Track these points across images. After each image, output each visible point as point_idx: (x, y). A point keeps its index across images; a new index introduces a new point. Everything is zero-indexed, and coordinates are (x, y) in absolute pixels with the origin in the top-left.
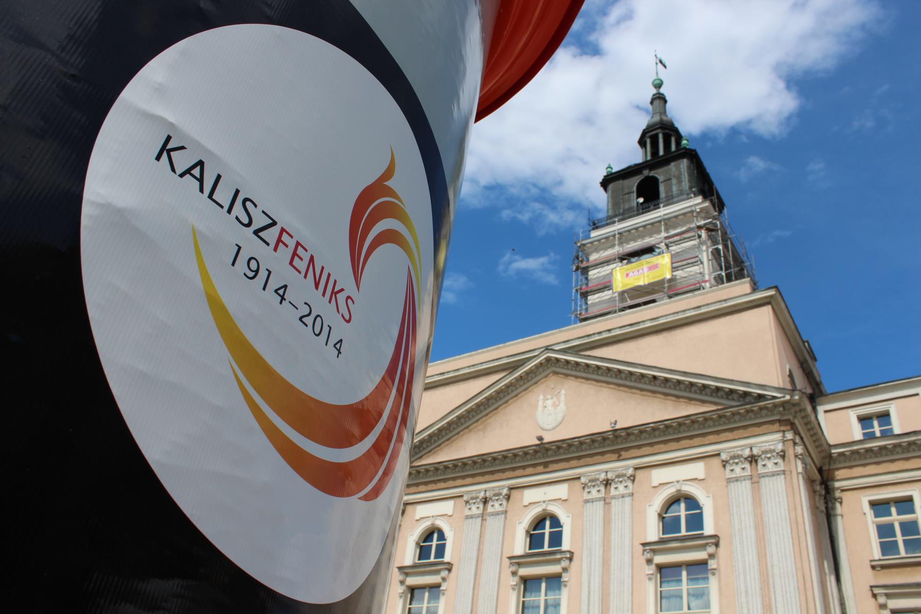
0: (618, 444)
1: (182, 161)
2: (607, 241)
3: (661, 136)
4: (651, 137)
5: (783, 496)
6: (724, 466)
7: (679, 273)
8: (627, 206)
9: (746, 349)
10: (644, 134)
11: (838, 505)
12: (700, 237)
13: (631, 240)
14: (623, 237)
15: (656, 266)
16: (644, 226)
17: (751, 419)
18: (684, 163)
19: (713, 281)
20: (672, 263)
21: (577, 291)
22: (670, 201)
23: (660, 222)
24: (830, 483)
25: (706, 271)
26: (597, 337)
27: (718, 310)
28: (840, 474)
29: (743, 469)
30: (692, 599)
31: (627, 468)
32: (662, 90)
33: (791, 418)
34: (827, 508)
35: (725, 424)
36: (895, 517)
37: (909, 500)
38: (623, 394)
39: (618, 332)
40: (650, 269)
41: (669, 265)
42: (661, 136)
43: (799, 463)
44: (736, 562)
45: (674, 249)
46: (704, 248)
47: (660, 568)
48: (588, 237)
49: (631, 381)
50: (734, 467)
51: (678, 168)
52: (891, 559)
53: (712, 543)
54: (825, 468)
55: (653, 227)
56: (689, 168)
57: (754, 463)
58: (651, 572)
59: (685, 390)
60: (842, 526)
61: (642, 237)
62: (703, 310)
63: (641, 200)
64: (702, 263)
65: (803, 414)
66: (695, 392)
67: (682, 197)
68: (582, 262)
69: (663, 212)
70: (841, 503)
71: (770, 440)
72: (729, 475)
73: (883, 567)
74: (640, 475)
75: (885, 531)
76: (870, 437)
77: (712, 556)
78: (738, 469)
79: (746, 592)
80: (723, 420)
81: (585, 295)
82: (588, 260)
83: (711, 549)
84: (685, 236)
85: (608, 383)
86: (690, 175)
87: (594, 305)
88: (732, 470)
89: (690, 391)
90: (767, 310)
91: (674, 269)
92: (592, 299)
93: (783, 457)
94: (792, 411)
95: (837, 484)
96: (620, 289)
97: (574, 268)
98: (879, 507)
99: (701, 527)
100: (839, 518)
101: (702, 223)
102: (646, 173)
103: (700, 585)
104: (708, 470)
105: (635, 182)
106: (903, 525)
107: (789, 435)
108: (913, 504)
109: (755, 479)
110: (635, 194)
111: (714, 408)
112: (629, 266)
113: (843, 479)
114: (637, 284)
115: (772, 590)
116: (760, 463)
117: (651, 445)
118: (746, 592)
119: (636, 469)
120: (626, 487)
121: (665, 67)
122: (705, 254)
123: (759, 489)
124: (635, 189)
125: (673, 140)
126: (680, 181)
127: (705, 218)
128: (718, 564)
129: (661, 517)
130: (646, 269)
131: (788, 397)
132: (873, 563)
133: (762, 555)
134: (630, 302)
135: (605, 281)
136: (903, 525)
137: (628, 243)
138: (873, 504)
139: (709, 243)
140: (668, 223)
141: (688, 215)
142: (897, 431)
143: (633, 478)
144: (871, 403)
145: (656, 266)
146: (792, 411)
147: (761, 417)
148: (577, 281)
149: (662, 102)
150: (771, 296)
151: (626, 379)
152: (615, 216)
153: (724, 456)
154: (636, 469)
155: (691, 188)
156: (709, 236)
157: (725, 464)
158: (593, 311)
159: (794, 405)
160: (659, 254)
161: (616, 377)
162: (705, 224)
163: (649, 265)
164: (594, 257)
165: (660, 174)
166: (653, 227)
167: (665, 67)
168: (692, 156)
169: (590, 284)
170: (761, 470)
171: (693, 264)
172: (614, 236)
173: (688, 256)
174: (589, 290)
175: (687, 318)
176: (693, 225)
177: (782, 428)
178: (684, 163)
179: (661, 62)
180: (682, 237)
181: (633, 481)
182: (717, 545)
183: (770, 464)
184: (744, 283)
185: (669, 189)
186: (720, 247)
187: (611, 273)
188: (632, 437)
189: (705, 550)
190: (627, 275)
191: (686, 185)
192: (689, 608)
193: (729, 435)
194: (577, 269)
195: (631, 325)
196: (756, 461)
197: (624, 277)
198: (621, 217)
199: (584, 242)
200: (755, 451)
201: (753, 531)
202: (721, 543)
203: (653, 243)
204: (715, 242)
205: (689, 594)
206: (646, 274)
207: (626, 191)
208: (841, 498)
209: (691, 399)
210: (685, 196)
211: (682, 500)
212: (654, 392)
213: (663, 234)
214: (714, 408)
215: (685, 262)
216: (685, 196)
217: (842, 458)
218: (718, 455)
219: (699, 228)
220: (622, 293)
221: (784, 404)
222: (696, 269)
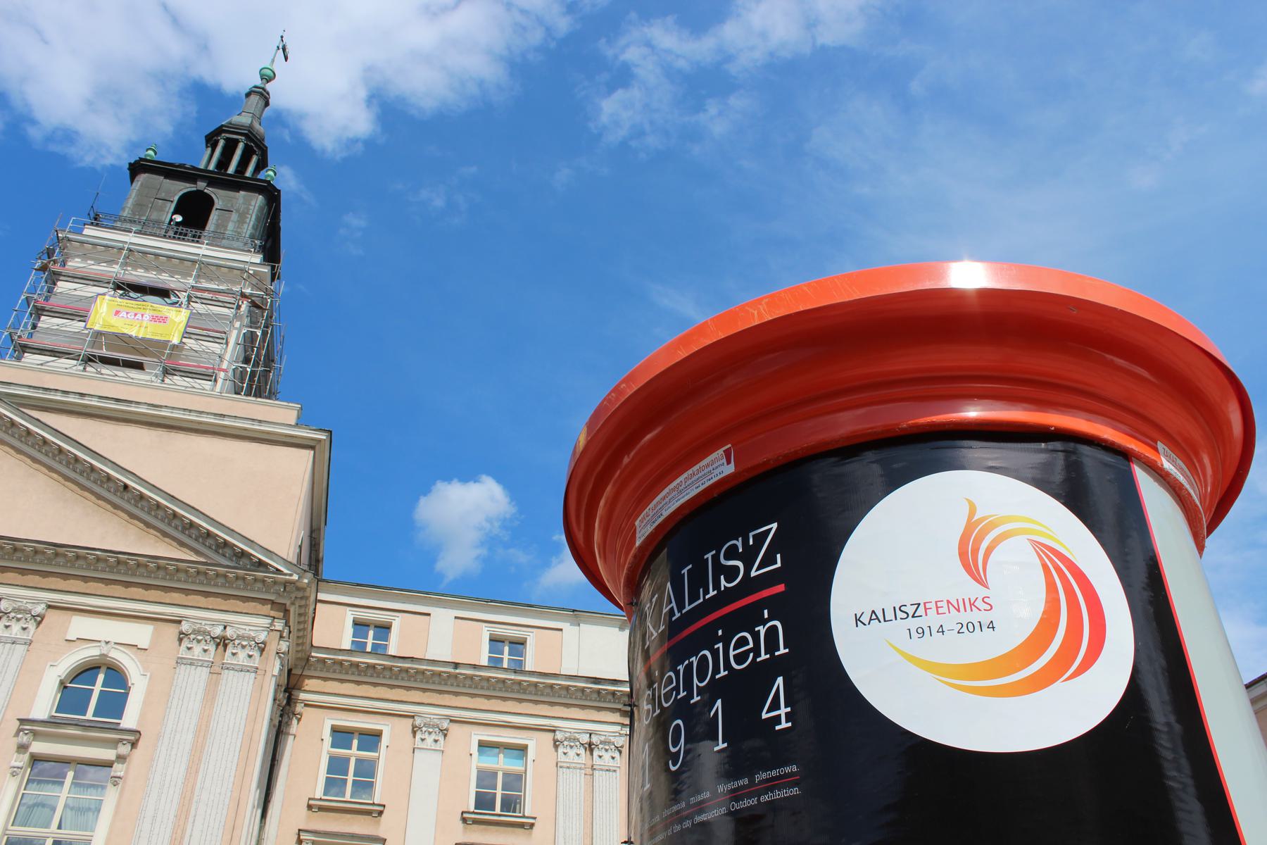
0: (34, 562)
1: (865, 619)
2: (108, 252)
3: (241, 146)
4: (227, 140)
5: (246, 697)
6: (180, 640)
7: (190, 343)
8: (154, 216)
9: (258, 492)
10: (220, 131)
11: (295, 721)
12: (239, 307)
13: (142, 267)
14: (133, 256)
15: (163, 320)
16: (169, 257)
17: (238, 588)
18: (258, 200)
19: (230, 373)
20: (187, 326)
21: (28, 300)
22: (218, 239)
23: (194, 262)
24: (295, 692)
25: (227, 357)
26: (59, 397)
27: (246, 429)
28: (310, 684)
29: (205, 651)
30: (69, 812)
31: (38, 602)
32: (269, 87)
33: (288, 603)
34: (280, 722)
35: (201, 583)
36: (354, 752)
37: (377, 735)
38: (69, 494)
39: (95, 402)
40: (155, 319)
41: (182, 327)
42: (241, 146)
43: (278, 662)
44: (156, 774)
45: (199, 307)
46: (237, 324)
47: (36, 759)
48: (80, 232)
49: (88, 479)
50: (194, 644)
51: (247, 202)
52: (334, 800)
53: (129, 741)
54: (296, 671)
55: (183, 264)
56: (261, 209)
57: (221, 647)
58: (20, 764)
59: (162, 520)
60: (290, 747)
61: (159, 270)
62: (226, 422)
63: (179, 218)
64: (227, 343)
65: (303, 602)
66: (176, 528)
67: (236, 244)
68: (55, 262)
69: (201, 250)
70: (299, 720)
71: (253, 624)
72: (183, 652)
73: (321, 809)
74: (52, 616)
75: (337, 766)
76: (359, 648)
77: (121, 758)
78: (197, 649)
79: (154, 817)
80: (202, 578)
81: (39, 312)
82: (64, 264)
83: (124, 749)
84: (221, 298)
85: (51, 469)
86: (258, 219)
87: (48, 331)
88: (189, 649)
89: (169, 524)
90: (308, 454)
91: (186, 334)
92: (46, 322)
93: (262, 650)
94: (293, 596)
95: (302, 696)
96: (97, 328)
97: (38, 264)
98: (341, 735)
99: (119, 712)
100: (291, 738)
101: (248, 291)
102: (201, 185)
103: (90, 796)
104: (155, 638)
105: (181, 188)
106: (359, 761)
107: (279, 625)
108: (380, 741)
109: (216, 669)
110: (173, 205)
111: (194, 558)
112: (125, 302)
113: (313, 689)
114: (126, 331)
115: (191, 820)
116: (230, 649)
117: (85, 579)
118: (154, 817)
119: (49, 607)
120: (24, 629)
121: (286, 59)
122: (235, 333)
123: (217, 684)
124: (176, 198)
125: (254, 159)
126: (242, 221)
127: (254, 286)
128: (126, 772)
129: (63, 686)
130: (147, 317)
131: (295, 577)
132: (312, 802)
133: (193, 770)
134: (104, 352)
135: (79, 305)
136: (359, 761)
137: (135, 267)
138: (335, 730)
139: (246, 321)
140: (205, 268)
141: (240, 272)
142: (392, 651)
143: (39, 620)
144: (374, 607)
145: (163, 320)
146: (293, 596)
147: (252, 590)
148: (34, 289)
149: (262, 103)
150: (319, 441)
151: (81, 473)
152: (132, 221)
153: (185, 627)
154: (49, 607)
155: (252, 237)
156: (249, 311)
157: (182, 636)
158: (39, 340)
159: (298, 589)
160: (174, 304)
161: (67, 465)
162: (252, 295)
163: (155, 314)
164: (75, 264)
165: (220, 197)
166: (183, 264)
167: (286, 59)
168: (272, 195)
169: (53, 300)
170: (228, 659)
171: (215, 340)
172: (122, 249)
173: (212, 326)
174: (48, 307)
175: (200, 423)
176: (236, 289)
177: (273, 613)
178: (258, 200)
179: (284, 49)
180: (214, 298)
181: (39, 623)
182: (134, 745)
183: (242, 655)
184: (293, 409)
185: (222, 225)
186: (259, 333)
187: (93, 299)
188: (61, 560)
189: (116, 748)
190: (117, 313)
191: (248, 228)
192: (60, 827)
193: (201, 601)
194: (44, 268)
195: (117, 400)
196: (225, 646)
197: (111, 315)
198: (139, 228)
199: (71, 236)
200: (229, 632)
201: (190, 736)
202: (141, 743)
203: (173, 286)
204: (253, 323)
205: (66, 806)
206: (145, 324)
207: (163, 195)
208: (301, 714)
209: (165, 534)
210: (240, 244)
211: (103, 669)
212: (116, 506)
213: (191, 281)
214: (194, 558)
215: (204, 333)
216: (240, 244)
217: (320, 666)
218: (179, 622)
219: (243, 295)
220: (99, 334)
221: (286, 584)
222: (216, 348)
